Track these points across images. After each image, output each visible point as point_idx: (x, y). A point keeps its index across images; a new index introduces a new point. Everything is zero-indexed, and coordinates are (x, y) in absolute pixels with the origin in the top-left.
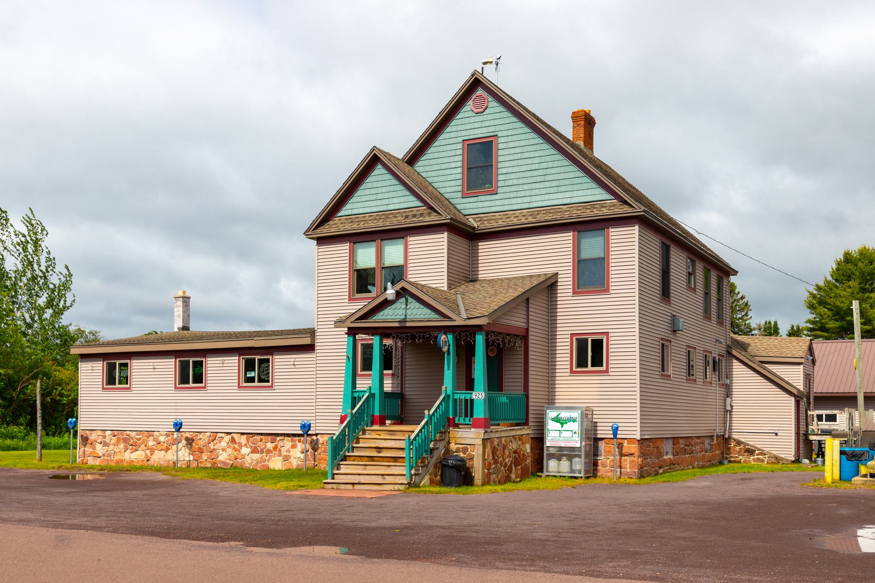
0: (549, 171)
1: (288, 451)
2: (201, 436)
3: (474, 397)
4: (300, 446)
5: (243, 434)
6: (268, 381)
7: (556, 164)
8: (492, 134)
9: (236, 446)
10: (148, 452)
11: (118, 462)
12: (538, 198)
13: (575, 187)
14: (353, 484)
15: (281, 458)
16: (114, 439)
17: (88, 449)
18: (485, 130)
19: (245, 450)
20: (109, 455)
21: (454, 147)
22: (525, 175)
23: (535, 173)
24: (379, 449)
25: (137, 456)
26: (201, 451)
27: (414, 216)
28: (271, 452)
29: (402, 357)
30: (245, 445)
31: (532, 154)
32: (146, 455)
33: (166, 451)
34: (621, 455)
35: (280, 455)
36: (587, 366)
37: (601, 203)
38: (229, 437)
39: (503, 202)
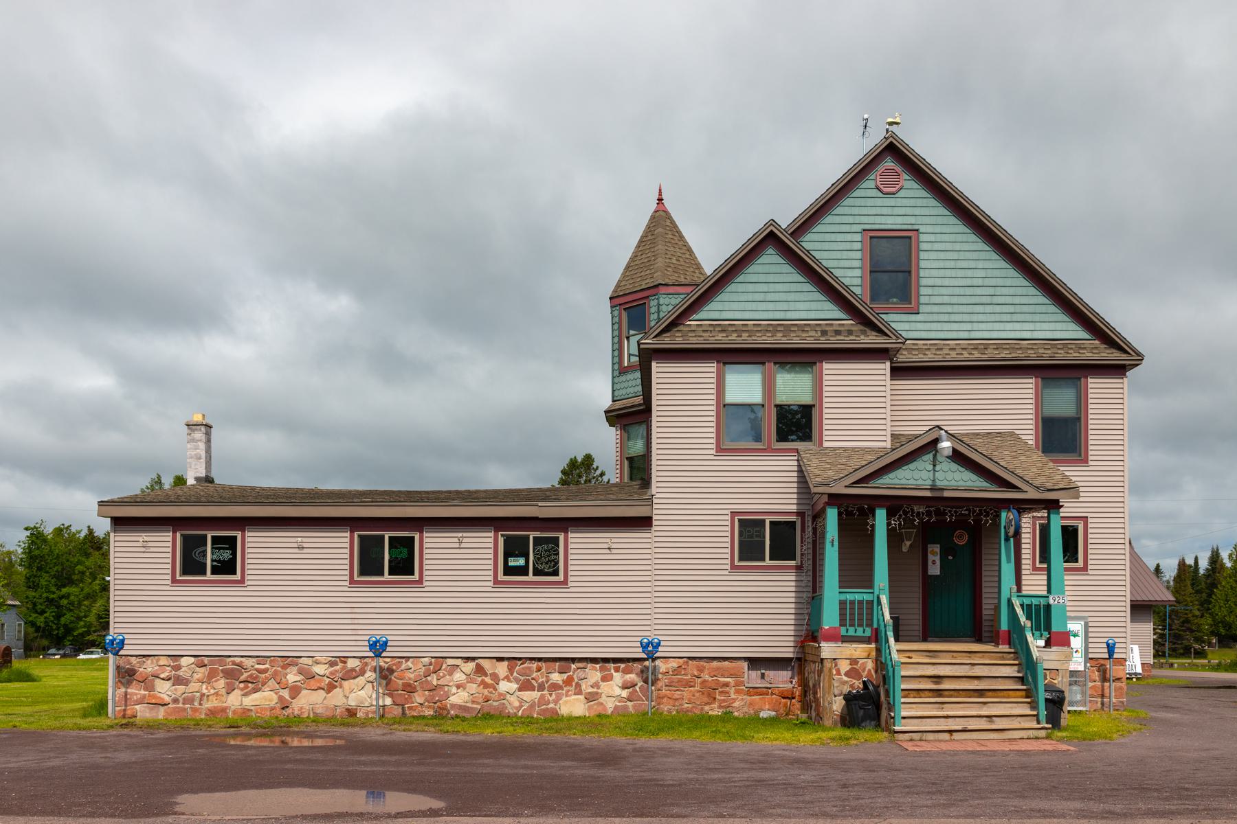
0: (999, 291)
1: (596, 685)
2: (409, 664)
3: (1051, 602)
4: (618, 677)
5: (500, 659)
6: (556, 573)
7: (1008, 282)
8: (909, 227)
9: (488, 680)
10: (286, 694)
11: (212, 712)
12: (983, 326)
13: (1037, 317)
14: (950, 732)
15: (582, 697)
16: (201, 673)
17: (136, 691)
18: (899, 220)
19: (504, 686)
20: (189, 700)
21: (849, 237)
22: (962, 291)
23: (979, 291)
24: (938, 678)
25: (263, 700)
26: (409, 689)
27: (838, 333)
28: (561, 688)
29: (814, 542)
30: (507, 678)
31: (972, 264)
32: (281, 698)
33: (329, 692)
34: (1104, 679)
35: (579, 692)
36: (763, 559)
37: (1065, 343)
38: (470, 666)
39: (927, 326)
